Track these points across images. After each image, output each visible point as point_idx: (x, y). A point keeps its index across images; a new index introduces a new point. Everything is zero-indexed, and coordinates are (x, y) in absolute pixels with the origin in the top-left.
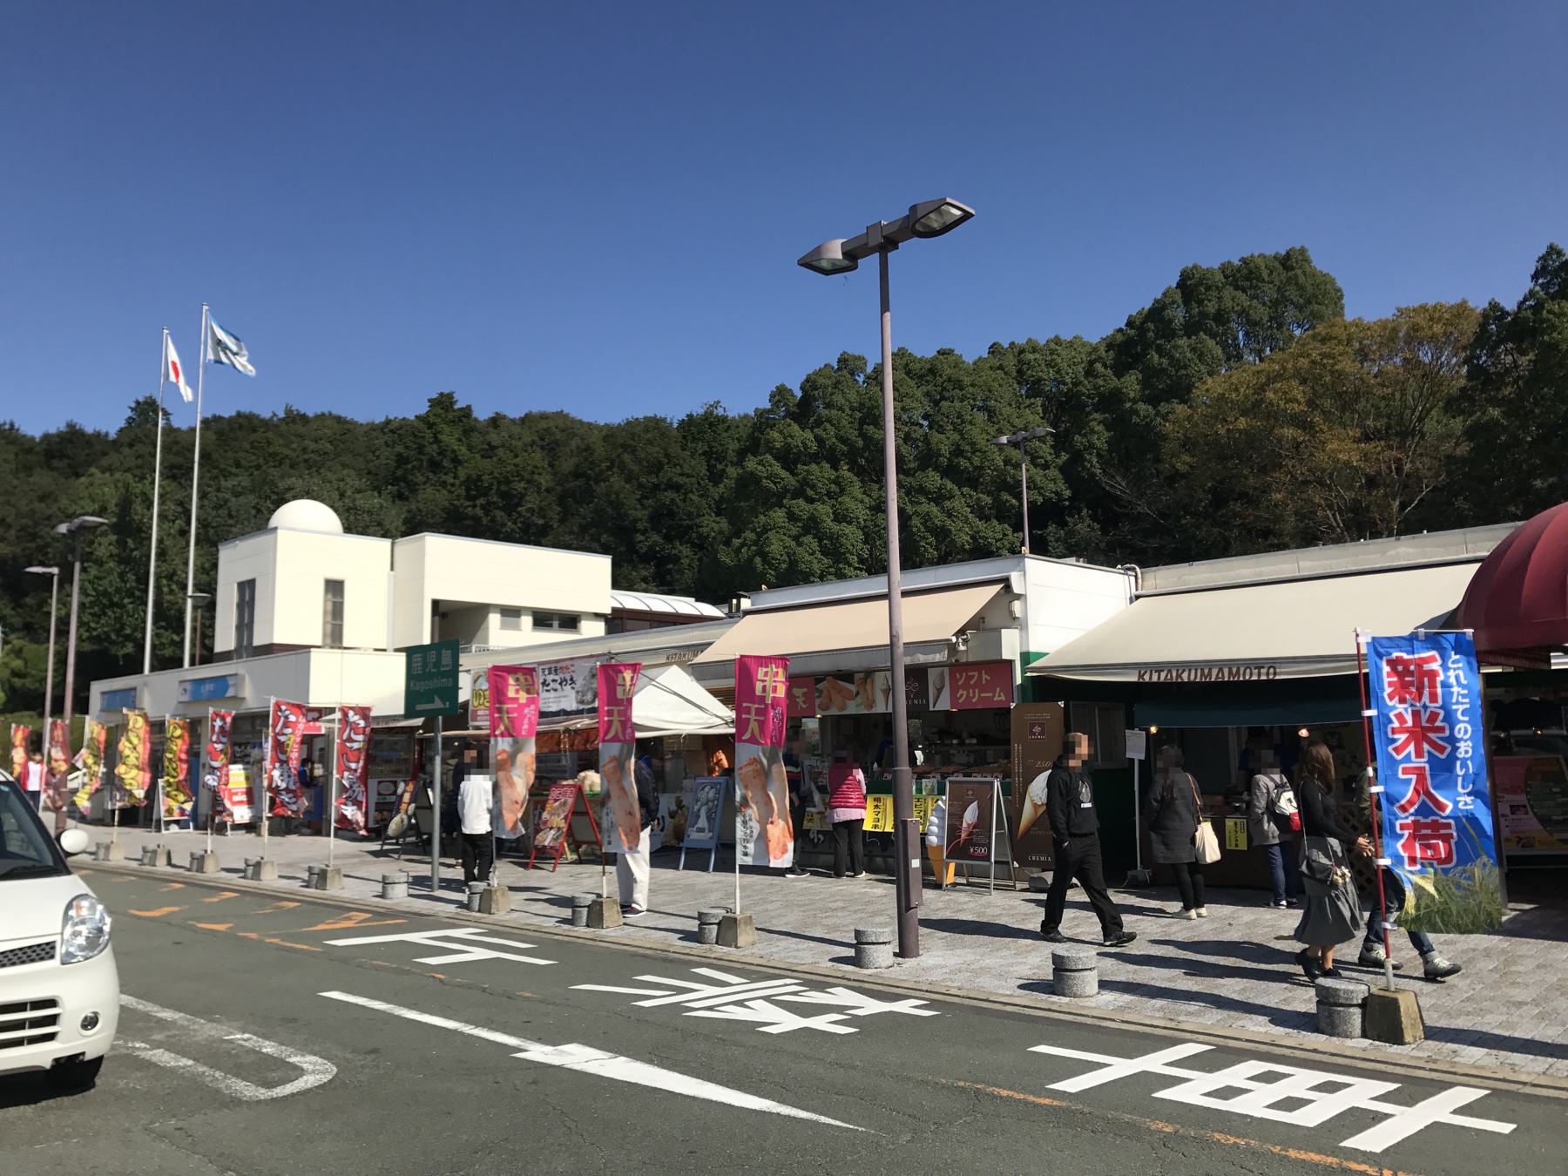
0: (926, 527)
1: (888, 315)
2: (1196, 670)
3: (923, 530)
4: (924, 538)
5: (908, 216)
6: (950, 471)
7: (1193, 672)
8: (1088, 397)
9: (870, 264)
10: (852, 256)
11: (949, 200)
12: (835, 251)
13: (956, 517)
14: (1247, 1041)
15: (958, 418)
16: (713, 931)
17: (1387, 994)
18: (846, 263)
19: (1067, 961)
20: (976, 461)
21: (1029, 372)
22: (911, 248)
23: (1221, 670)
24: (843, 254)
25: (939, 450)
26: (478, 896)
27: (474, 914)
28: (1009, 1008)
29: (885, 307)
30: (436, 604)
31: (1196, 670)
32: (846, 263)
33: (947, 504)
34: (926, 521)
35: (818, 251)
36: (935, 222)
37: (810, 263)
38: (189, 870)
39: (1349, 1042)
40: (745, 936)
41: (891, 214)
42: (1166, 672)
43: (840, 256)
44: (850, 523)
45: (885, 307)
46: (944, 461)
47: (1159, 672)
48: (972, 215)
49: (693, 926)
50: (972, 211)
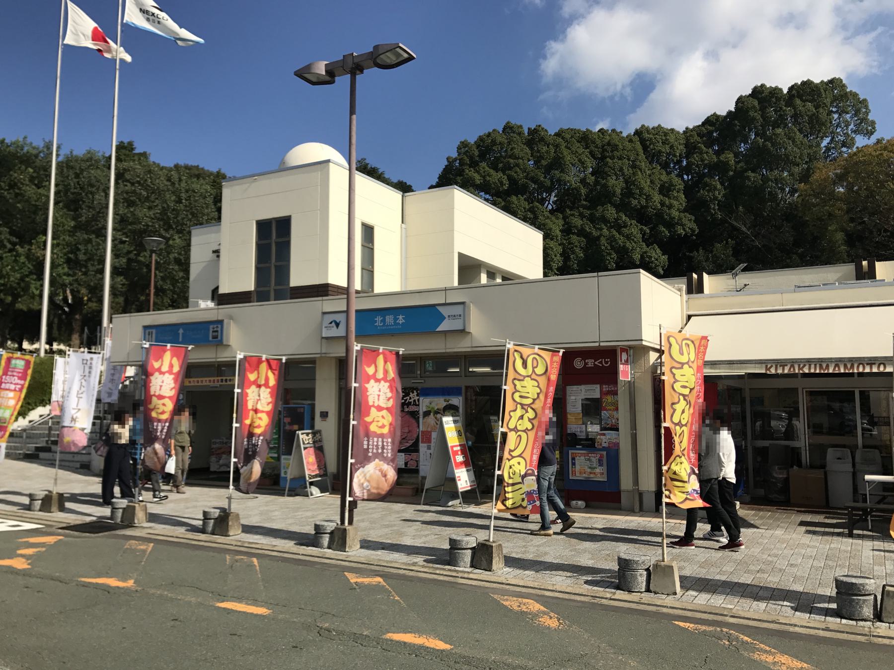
0: (611, 246)
1: (354, 117)
2: (815, 365)
3: (609, 248)
4: (610, 254)
5: (372, 52)
6: (622, 207)
7: (813, 366)
8: (697, 166)
9: (343, 81)
10: (331, 74)
11: (401, 45)
12: (320, 68)
13: (633, 240)
14: (303, 555)
15: (619, 171)
16: (326, 540)
17: (487, 543)
18: (328, 78)
19: (321, 527)
20: (643, 202)
21: (652, 146)
22: (371, 74)
23: (792, 366)
24: (326, 71)
25: (615, 192)
26: (213, 521)
27: (36, 513)
28: (194, 542)
29: (352, 112)
30: (461, 256)
31: (815, 365)
32: (328, 78)
33: (625, 230)
34: (612, 241)
35: (308, 68)
36: (390, 58)
37: (303, 74)
38: (203, 531)
39: (634, 597)
40: (497, 563)
41: (360, 48)
42: (789, 366)
43: (324, 73)
44: (552, 239)
45: (352, 112)
46: (617, 199)
47: (783, 366)
48: (411, 58)
49: (26, 501)
50: (415, 56)
